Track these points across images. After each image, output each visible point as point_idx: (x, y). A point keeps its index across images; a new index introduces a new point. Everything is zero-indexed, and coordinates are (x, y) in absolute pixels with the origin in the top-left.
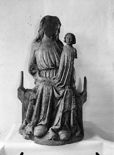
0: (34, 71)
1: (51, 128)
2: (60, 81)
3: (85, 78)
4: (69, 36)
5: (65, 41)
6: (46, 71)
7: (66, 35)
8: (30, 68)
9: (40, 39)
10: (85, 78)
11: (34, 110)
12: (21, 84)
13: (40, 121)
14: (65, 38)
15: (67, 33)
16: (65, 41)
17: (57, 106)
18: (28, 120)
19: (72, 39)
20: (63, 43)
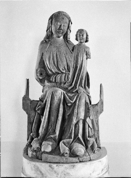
1: (62, 141)
10: (101, 86)
14: (77, 35)
15: (79, 30)
17: (69, 115)
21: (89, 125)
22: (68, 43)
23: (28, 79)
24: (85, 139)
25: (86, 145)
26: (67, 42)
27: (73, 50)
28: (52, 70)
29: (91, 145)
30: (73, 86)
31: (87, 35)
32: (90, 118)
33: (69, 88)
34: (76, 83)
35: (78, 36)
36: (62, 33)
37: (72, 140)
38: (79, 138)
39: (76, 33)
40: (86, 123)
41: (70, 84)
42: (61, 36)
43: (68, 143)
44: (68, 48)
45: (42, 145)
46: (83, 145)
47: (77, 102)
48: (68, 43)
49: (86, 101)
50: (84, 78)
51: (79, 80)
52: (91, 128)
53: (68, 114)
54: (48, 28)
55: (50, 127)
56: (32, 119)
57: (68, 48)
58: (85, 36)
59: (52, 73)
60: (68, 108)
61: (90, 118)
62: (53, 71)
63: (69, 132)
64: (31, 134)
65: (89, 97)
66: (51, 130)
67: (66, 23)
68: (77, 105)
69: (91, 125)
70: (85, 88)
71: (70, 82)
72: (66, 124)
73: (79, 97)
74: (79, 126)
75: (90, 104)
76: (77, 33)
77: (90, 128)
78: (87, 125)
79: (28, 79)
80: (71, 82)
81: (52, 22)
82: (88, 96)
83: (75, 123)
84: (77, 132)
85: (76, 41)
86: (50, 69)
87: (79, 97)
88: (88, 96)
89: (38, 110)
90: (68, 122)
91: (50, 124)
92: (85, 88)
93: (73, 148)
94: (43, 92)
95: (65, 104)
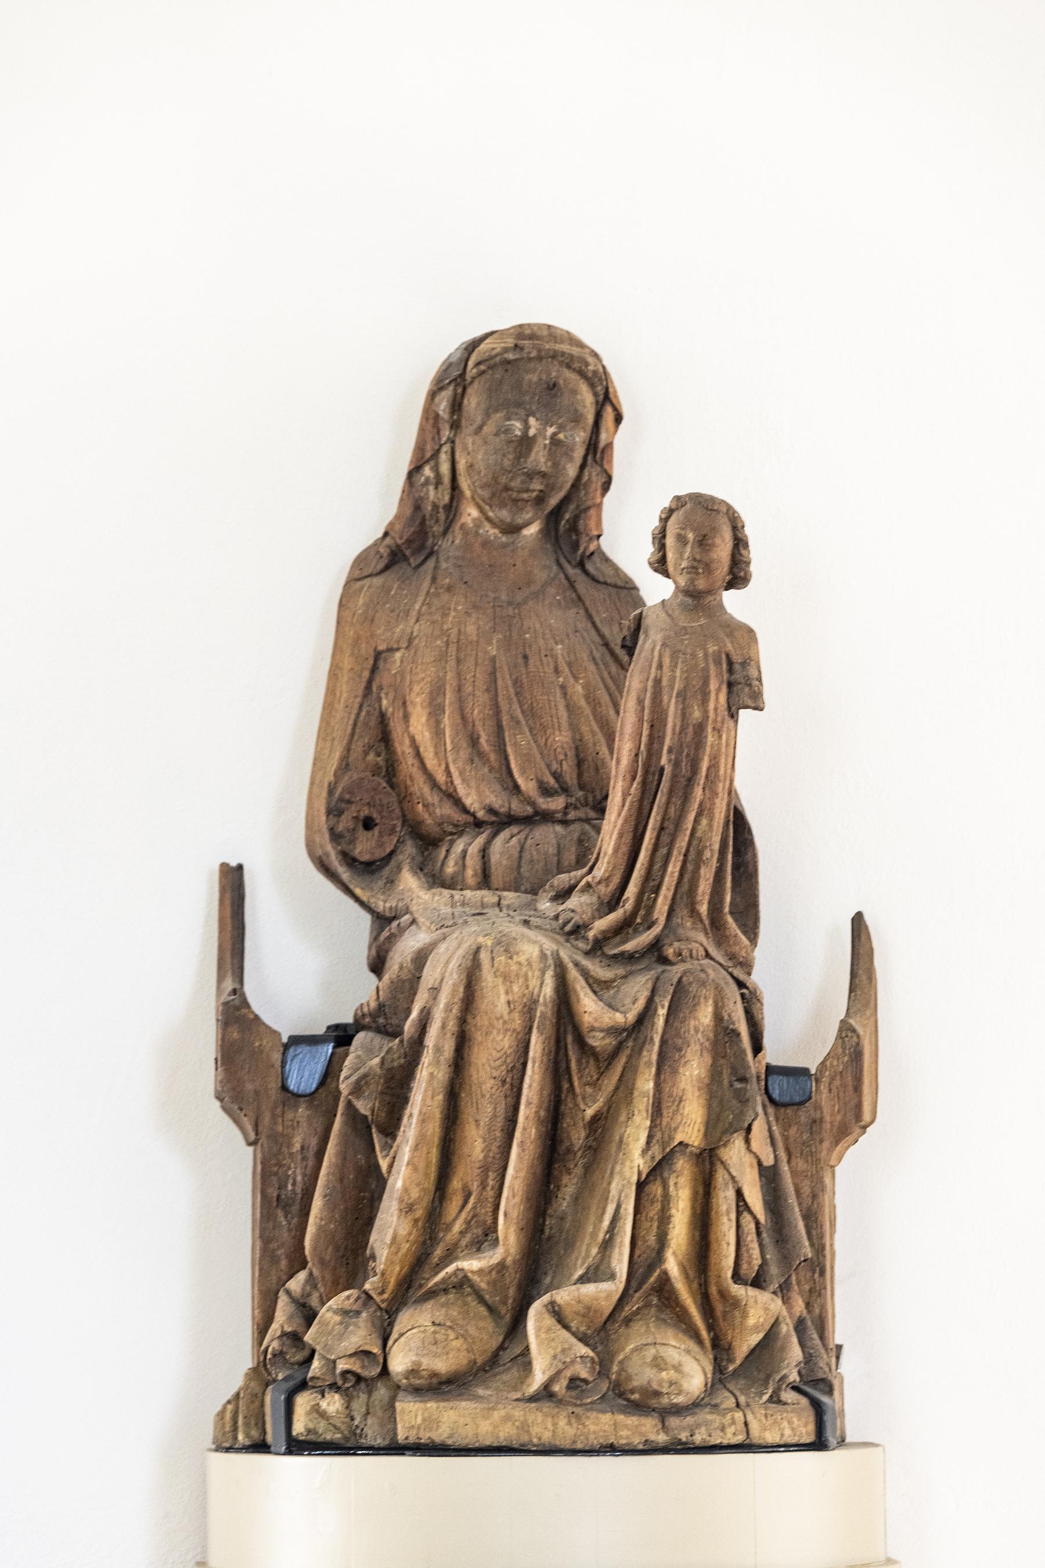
0: (365, 847)
1: (546, 1298)
2: (613, 903)
3: (858, 922)
4: (764, 1284)
5: (660, 565)
6: (480, 840)
7: (670, 512)
8: (340, 813)
9: (422, 547)
10: (858, 922)
11: (382, 1182)
12: (220, 1031)
13: (450, 1256)
14: (660, 538)
15: (678, 498)
16: (660, 565)
17: (596, 1118)
18: (567, 526)
19: (839, 1348)
20: (635, 588)
21: (739, 1194)
22: (586, 573)
23: (240, 867)
24: (713, 1290)
25: (716, 1343)
26: (581, 565)
27: (630, 648)
28: (461, 790)
29: (755, 1339)
30: (629, 906)
31: (740, 543)
32: (747, 1141)
33: (602, 924)
34: (651, 885)
35: (670, 541)
36: (540, 500)
37: (614, 1288)
38: (665, 1282)
39: (656, 523)
40: (721, 1176)
41: (605, 891)
42: (527, 524)
43: (588, 1311)
44: (589, 617)
45: (394, 1336)
46: (700, 1342)
47: (660, 1022)
48: (586, 573)
49: (718, 1017)
50: (711, 855)
51: (674, 868)
52: (762, 1218)
53: (590, 1112)
54: (420, 448)
55: (453, 1206)
56: (297, 1175)
57: (589, 617)
58: (723, 551)
59: (556, 786)
60: (591, 1070)
61: (747, 1141)
62: (468, 802)
63: (594, 1235)
64: (297, 1283)
65: (750, 1000)
66: (457, 1227)
67: (577, 419)
68: (657, 1039)
69: (755, 1198)
70: (716, 925)
71: (606, 880)
72: (569, 1186)
73: (682, 842)
74: (666, 1198)
75: (757, 1047)
76: (665, 520)
77: (747, 1219)
78: (731, 1194)
79: (240, 867)
80: (616, 880)
81: (457, 406)
82: (741, 984)
83: (640, 1173)
84: (652, 1239)
85: (659, 577)
86: (441, 778)
87: (682, 842)
88: (741, 984)
89: (357, 1089)
90: (588, 1169)
91: (456, 1184)
92: (716, 925)
93: (618, 1352)
94: (377, 966)
95: (570, 1039)
